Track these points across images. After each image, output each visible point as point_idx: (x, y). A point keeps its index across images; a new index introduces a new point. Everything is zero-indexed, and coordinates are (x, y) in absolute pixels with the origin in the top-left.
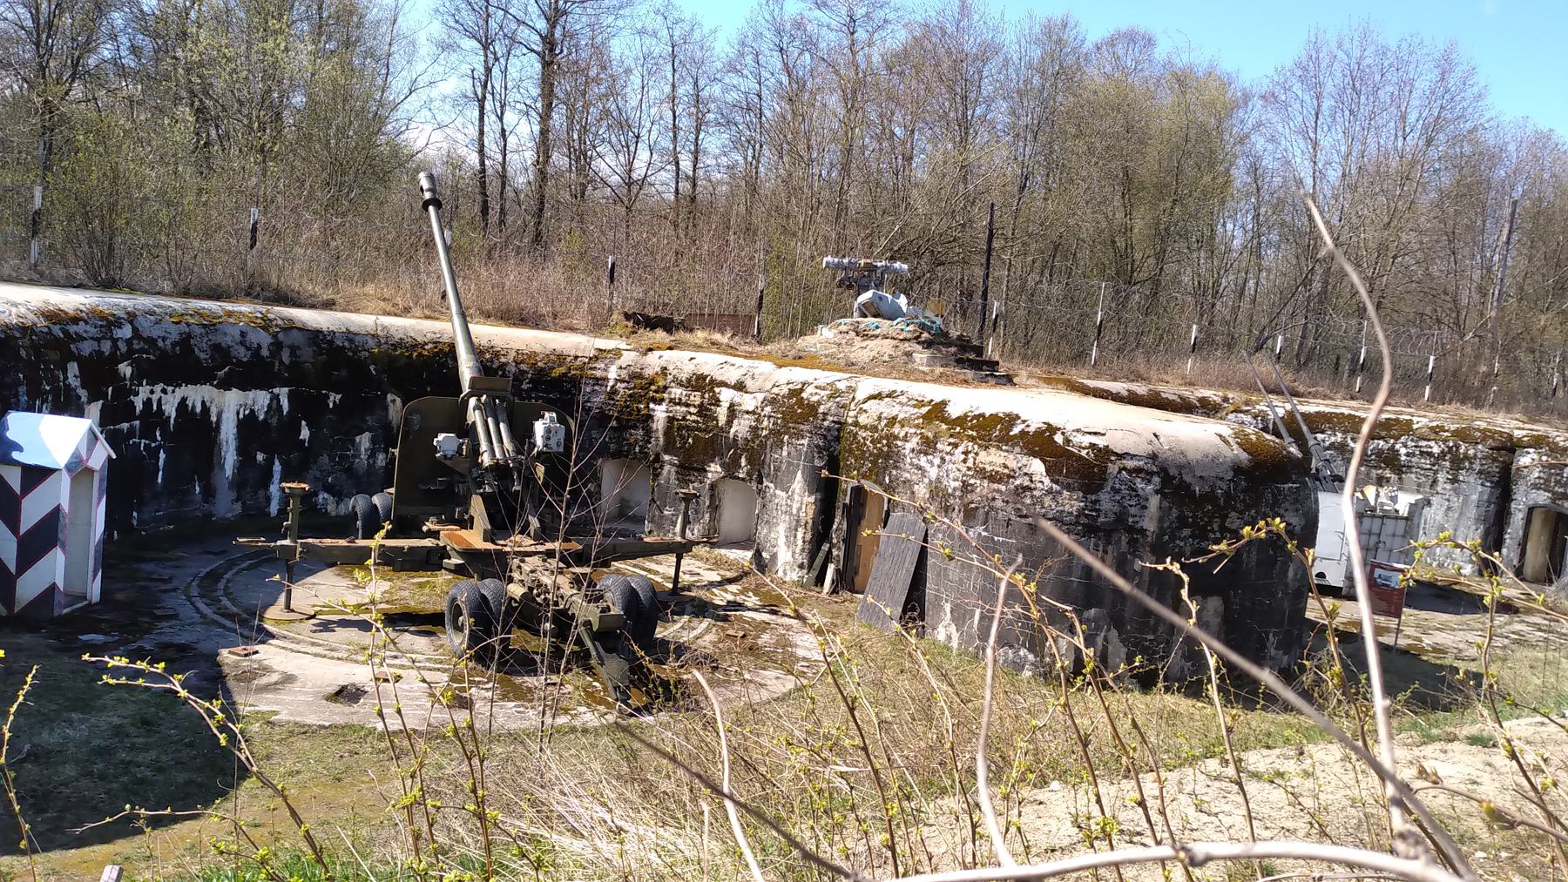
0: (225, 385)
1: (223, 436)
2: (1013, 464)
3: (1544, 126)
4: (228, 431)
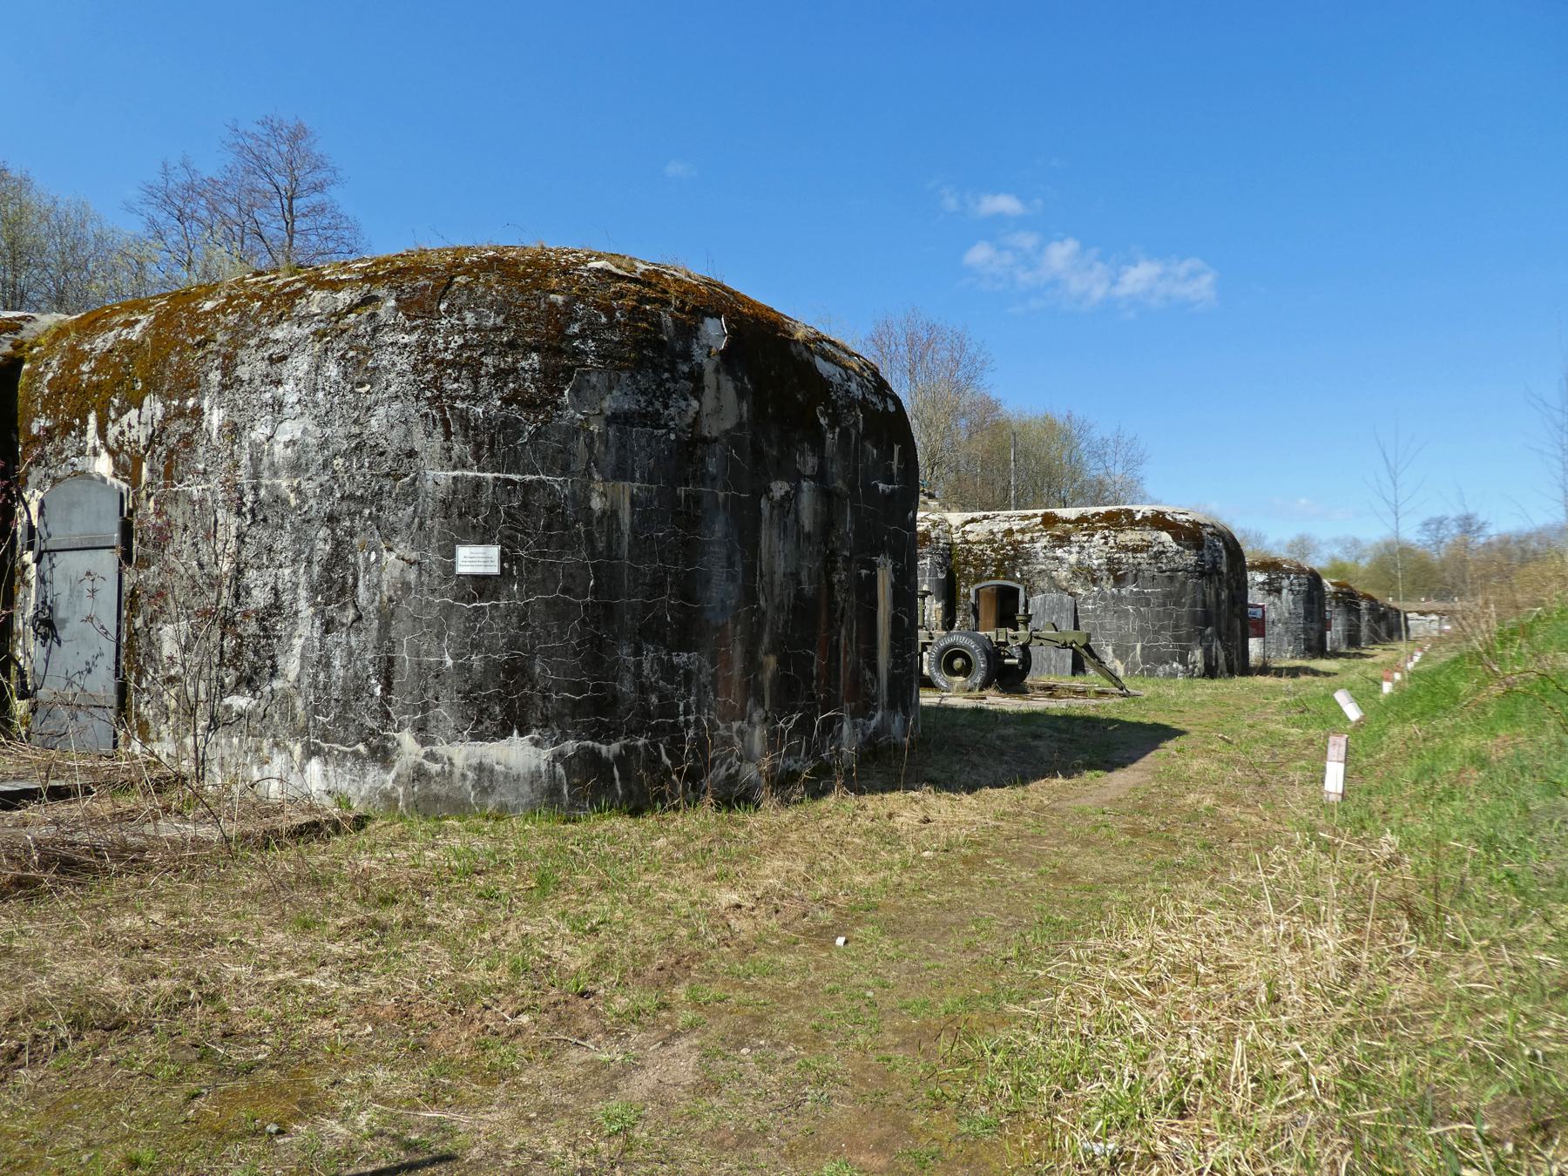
2: (1149, 538)
3: (994, 395)
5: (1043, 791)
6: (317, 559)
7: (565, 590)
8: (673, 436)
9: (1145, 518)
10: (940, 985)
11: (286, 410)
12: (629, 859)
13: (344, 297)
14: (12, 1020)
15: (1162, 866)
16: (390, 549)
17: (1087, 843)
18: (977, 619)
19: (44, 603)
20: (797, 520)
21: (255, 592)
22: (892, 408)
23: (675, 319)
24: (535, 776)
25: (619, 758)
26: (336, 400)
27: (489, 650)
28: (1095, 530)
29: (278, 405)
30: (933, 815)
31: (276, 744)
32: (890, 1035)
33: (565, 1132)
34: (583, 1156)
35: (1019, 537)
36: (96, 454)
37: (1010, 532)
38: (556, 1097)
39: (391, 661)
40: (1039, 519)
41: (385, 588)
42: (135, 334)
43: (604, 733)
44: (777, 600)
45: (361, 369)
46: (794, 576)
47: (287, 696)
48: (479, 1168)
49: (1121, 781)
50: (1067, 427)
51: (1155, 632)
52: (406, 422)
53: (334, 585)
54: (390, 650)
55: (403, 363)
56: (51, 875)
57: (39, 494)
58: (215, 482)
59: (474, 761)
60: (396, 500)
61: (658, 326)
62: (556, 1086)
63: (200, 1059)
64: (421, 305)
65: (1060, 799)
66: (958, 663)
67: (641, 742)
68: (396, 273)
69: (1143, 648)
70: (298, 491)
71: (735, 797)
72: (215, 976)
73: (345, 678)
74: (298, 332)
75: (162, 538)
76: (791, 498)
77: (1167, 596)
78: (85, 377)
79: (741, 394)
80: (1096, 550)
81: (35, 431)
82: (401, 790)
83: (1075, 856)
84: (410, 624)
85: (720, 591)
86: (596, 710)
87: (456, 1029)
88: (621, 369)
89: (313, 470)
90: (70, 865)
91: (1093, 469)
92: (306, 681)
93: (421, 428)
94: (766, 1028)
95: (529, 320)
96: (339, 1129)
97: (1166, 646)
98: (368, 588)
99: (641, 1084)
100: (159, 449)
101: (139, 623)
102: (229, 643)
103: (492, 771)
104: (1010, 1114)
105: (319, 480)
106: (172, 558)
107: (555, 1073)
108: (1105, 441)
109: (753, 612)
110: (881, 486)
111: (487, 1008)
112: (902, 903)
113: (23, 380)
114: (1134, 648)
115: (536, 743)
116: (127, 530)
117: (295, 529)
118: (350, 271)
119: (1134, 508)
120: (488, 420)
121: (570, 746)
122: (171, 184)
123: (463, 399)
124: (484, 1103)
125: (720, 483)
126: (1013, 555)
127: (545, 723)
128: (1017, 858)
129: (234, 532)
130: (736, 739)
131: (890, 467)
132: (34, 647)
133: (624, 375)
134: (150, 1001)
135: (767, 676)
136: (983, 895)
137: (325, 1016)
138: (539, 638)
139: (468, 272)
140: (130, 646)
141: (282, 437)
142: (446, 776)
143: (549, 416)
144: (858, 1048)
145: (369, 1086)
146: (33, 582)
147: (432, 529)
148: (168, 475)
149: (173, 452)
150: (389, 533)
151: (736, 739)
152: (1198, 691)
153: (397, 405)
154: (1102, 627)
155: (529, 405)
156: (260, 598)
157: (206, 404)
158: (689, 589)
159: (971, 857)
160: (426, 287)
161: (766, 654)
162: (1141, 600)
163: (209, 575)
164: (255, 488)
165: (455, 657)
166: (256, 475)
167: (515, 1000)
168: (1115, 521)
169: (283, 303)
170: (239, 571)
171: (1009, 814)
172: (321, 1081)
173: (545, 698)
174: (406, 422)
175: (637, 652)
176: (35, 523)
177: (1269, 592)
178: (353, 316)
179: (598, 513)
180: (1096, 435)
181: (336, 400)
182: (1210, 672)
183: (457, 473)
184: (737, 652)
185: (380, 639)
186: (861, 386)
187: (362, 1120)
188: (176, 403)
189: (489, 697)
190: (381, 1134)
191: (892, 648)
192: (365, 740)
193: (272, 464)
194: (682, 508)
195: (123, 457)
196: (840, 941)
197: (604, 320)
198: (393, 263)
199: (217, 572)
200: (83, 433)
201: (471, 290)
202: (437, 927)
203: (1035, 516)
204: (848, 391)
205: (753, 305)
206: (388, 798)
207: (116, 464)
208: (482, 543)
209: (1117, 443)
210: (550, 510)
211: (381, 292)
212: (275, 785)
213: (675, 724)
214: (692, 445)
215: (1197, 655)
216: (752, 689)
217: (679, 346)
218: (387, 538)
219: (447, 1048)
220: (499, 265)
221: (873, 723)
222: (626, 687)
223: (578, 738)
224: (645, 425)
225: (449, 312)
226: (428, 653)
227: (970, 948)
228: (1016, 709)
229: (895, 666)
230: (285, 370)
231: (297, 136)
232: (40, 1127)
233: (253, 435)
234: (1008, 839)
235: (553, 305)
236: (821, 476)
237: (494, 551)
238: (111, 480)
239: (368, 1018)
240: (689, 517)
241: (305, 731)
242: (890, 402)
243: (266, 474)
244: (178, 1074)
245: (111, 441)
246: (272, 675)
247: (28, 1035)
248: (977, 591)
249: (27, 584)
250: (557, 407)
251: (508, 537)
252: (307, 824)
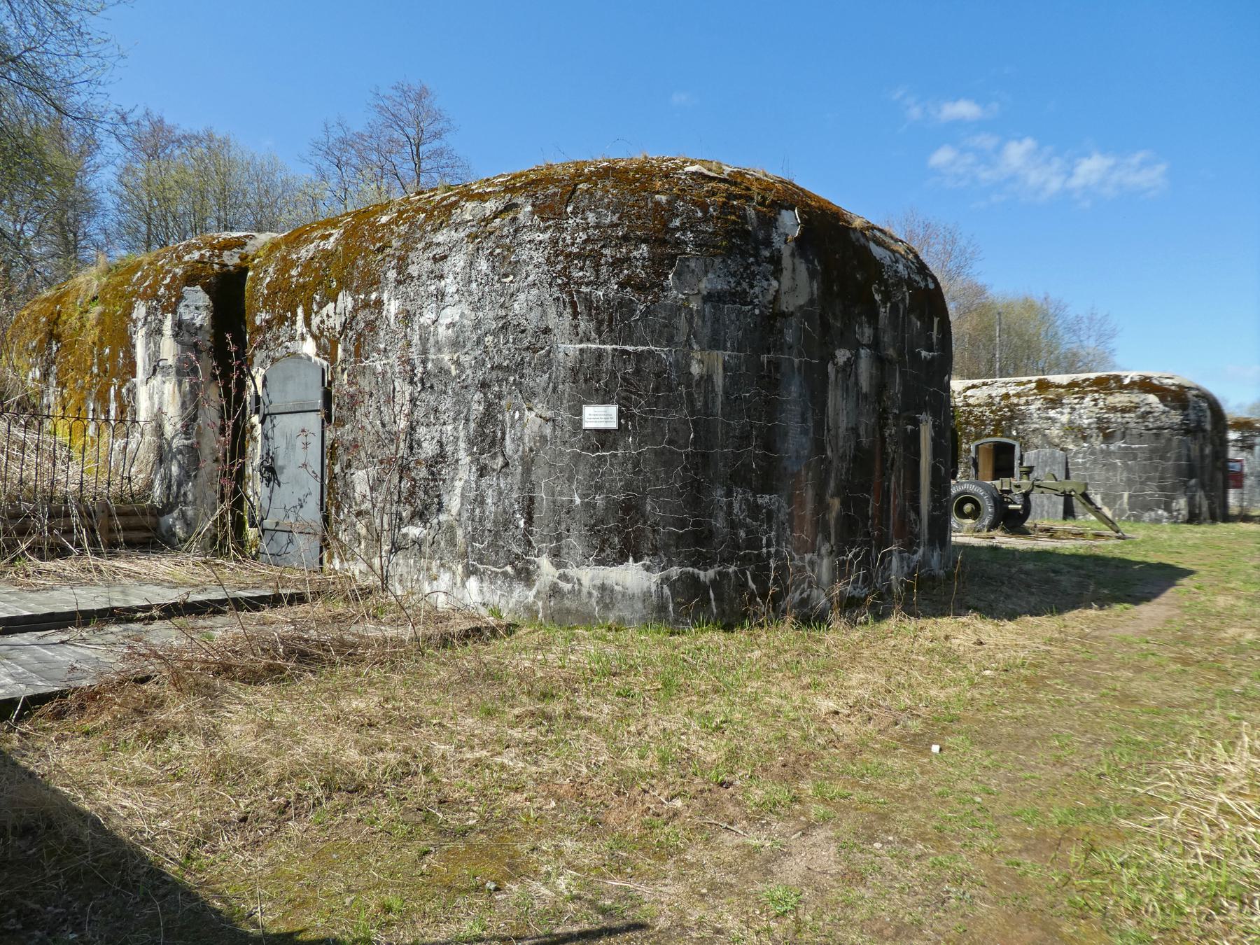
2: (1136, 400)
3: (981, 280)
5: (1080, 620)
6: (473, 417)
7: (670, 442)
8: (757, 312)
9: (1133, 383)
10: (1042, 795)
11: (447, 299)
12: (733, 668)
13: (491, 206)
14: (281, 780)
15: (1222, 694)
16: (530, 409)
17: (1139, 670)
18: (977, 471)
19: (268, 454)
20: (857, 383)
21: (425, 445)
22: (932, 286)
23: (758, 212)
24: (646, 595)
25: (713, 582)
26: (486, 289)
27: (609, 491)
28: (1086, 393)
29: (441, 295)
30: (984, 638)
31: (442, 565)
32: (1010, 841)
33: (736, 910)
34: (758, 933)
35: (1015, 400)
36: (303, 339)
37: (1007, 396)
38: (721, 877)
39: (532, 500)
40: (1033, 385)
41: (526, 440)
42: (330, 244)
43: (702, 561)
44: (841, 451)
45: (505, 263)
46: (854, 430)
47: (451, 528)
48: (670, 938)
49: (1150, 613)
50: (1045, 307)
51: (1142, 483)
52: (542, 305)
53: (487, 438)
54: (531, 490)
55: (539, 257)
56: (291, 664)
57: (262, 371)
58: (393, 359)
59: (598, 582)
60: (535, 369)
61: (744, 217)
62: (718, 866)
63: (424, 821)
64: (552, 208)
65: (1099, 628)
66: (968, 507)
67: (732, 569)
68: (530, 184)
69: (1130, 497)
70: (457, 363)
71: (811, 618)
72: (428, 751)
73: (496, 513)
74: (455, 236)
75: (354, 402)
76: (852, 364)
77: (1153, 451)
78: (294, 279)
79: (812, 274)
80: (1087, 410)
81: (258, 323)
82: (540, 604)
83: (1131, 680)
84: (547, 469)
85: (795, 442)
86: (695, 542)
87: (624, 809)
88: (715, 256)
89: (469, 346)
90: (305, 656)
91: (1068, 343)
92: (465, 515)
93: (554, 309)
94: (892, 825)
95: (639, 217)
96: (544, 891)
97: (1151, 495)
98: (513, 440)
99: (793, 868)
100: (351, 334)
101: (337, 469)
102: (406, 485)
103: (612, 591)
104: (1162, 931)
105: (473, 354)
106: (364, 419)
107: (715, 854)
108: (1079, 320)
109: (822, 461)
110: (924, 353)
111: (645, 791)
112: (980, 716)
113: (248, 284)
114: (1121, 497)
115: (648, 569)
116: (327, 397)
117: (456, 394)
118: (493, 184)
119: (1123, 374)
120: (608, 301)
121: (675, 572)
122: (331, 139)
123: (587, 285)
124: (659, 876)
125: (795, 351)
126: (1010, 415)
127: (655, 552)
128: (1073, 680)
129: (408, 398)
130: (808, 568)
131: (930, 337)
132: (261, 488)
133: (718, 261)
134: (380, 770)
135: (832, 516)
136: (1054, 713)
137: (516, 790)
138: (649, 481)
139: (588, 180)
140: (331, 487)
141: (445, 321)
142: (576, 593)
143: (657, 296)
144: (984, 850)
145: (561, 854)
146: (259, 438)
147: (563, 392)
148: (357, 354)
149: (360, 336)
150: (530, 396)
151: (808, 568)
152: (1188, 535)
153: (535, 291)
154: (1091, 477)
155: (640, 288)
156: (429, 449)
157: (385, 297)
158: (770, 440)
159: (1031, 678)
160: (555, 194)
161: (832, 497)
162: (1127, 454)
163: (389, 432)
164: (424, 362)
165: (582, 496)
166: (424, 351)
167: (667, 786)
168: (1103, 385)
169: (442, 213)
170: (412, 428)
171: (1056, 640)
172: (523, 847)
173: (654, 531)
174: (542, 305)
175: (729, 494)
176: (260, 393)
177: (1242, 449)
178: (498, 220)
179: (697, 377)
180: (1071, 313)
181: (486, 289)
182: (1193, 518)
183: (583, 346)
184: (809, 494)
185: (523, 482)
186: (907, 267)
187: (562, 884)
188: (362, 297)
189: (610, 530)
190: (579, 898)
191: (932, 493)
192: (512, 563)
193: (437, 342)
194: (765, 373)
195: (323, 341)
196: (935, 748)
197: (700, 214)
198: (527, 176)
199: (395, 429)
200: (294, 323)
201: (592, 194)
202: (590, 719)
203: (1030, 382)
204: (896, 271)
205: (819, 200)
206: (531, 611)
207: (318, 346)
208: (604, 403)
209: (1091, 319)
210: (658, 375)
211: (520, 200)
212: (442, 598)
213: (759, 555)
214: (772, 319)
215: (1181, 504)
216: (821, 526)
217: (761, 235)
218: (528, 400)
219: (620, 825)
220: (608, 172)
221: (917, 557)
222: (719, 523)
223: (681, 565)
224: (735, 303)
225: (574, 213)
226: (561, 494)
227: (1059, 762)
228: (1024, 547)
229: (934, 509)
230: (446, 266)
231: (420, 96)
232: (310, 872)
233: (422, 320)
234: (1061, 662)
235: (658, 203)
236: (875, 345)
237: (613, 410)
238: (315, 358)
239: (552, 794)
240: (770, 379)
241: (465, 555)
242: (930, 280)
243: (432, 350)
244: (410, 833)
245: (314, 328)
246: (439, 510)
247: (292, 793)
248: (977, 447)
249: (255, 439)
250: (663, 290)
251: (624, 398)
252: (472, 630)
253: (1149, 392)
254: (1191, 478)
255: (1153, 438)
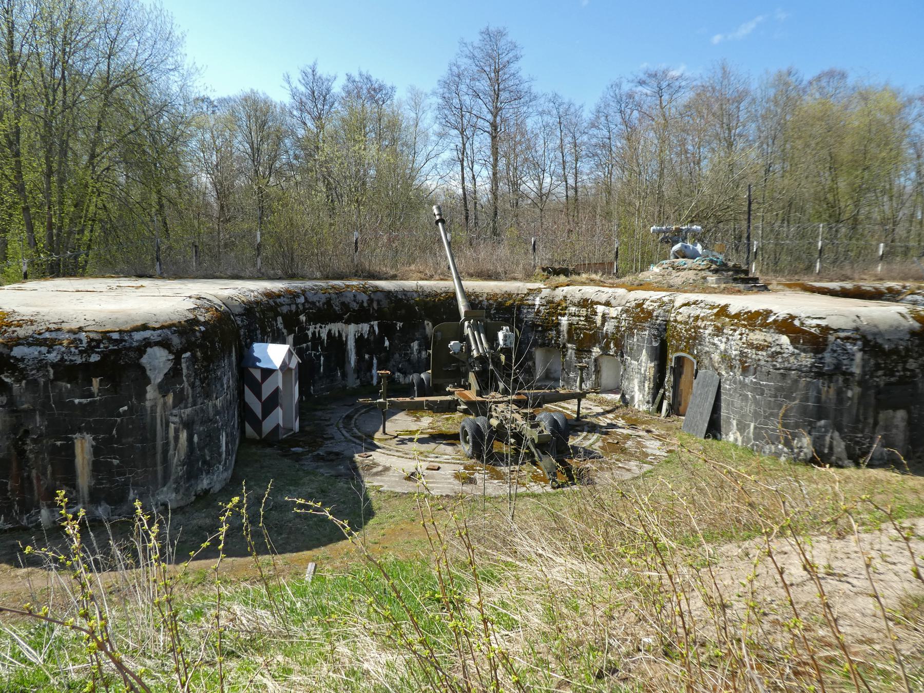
0: (348, 322)
1: (349, 347)
2: (770, 339)
4: (351, 345)
51: (766, 417)
69: (755, 428)
77: (778, 389)
114: (749, 426)
162: (758, 389)
215: (805, 442)
253: (783, 333)
254: (820, 419)
255: (779, 377)
